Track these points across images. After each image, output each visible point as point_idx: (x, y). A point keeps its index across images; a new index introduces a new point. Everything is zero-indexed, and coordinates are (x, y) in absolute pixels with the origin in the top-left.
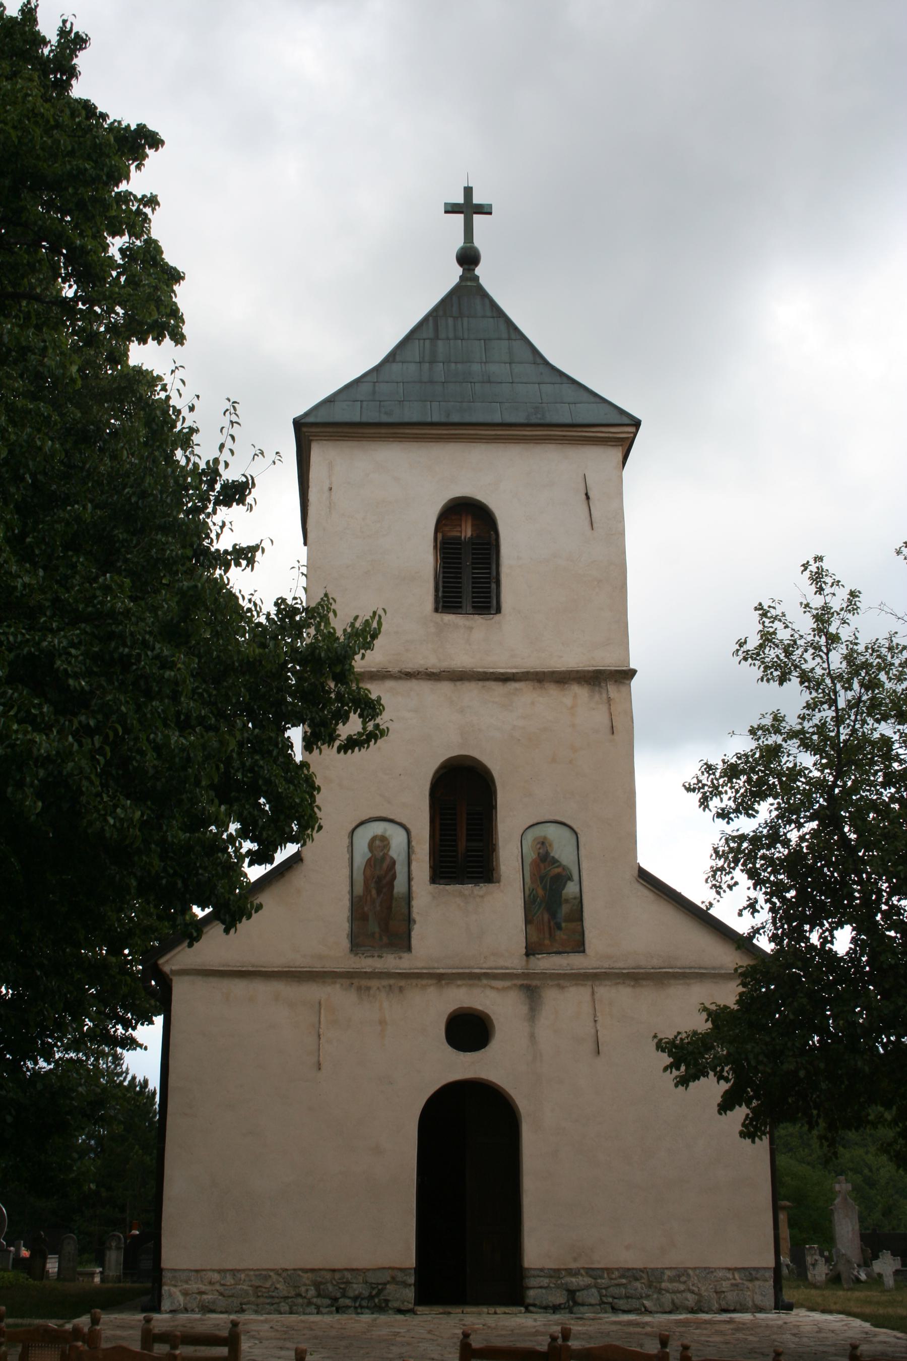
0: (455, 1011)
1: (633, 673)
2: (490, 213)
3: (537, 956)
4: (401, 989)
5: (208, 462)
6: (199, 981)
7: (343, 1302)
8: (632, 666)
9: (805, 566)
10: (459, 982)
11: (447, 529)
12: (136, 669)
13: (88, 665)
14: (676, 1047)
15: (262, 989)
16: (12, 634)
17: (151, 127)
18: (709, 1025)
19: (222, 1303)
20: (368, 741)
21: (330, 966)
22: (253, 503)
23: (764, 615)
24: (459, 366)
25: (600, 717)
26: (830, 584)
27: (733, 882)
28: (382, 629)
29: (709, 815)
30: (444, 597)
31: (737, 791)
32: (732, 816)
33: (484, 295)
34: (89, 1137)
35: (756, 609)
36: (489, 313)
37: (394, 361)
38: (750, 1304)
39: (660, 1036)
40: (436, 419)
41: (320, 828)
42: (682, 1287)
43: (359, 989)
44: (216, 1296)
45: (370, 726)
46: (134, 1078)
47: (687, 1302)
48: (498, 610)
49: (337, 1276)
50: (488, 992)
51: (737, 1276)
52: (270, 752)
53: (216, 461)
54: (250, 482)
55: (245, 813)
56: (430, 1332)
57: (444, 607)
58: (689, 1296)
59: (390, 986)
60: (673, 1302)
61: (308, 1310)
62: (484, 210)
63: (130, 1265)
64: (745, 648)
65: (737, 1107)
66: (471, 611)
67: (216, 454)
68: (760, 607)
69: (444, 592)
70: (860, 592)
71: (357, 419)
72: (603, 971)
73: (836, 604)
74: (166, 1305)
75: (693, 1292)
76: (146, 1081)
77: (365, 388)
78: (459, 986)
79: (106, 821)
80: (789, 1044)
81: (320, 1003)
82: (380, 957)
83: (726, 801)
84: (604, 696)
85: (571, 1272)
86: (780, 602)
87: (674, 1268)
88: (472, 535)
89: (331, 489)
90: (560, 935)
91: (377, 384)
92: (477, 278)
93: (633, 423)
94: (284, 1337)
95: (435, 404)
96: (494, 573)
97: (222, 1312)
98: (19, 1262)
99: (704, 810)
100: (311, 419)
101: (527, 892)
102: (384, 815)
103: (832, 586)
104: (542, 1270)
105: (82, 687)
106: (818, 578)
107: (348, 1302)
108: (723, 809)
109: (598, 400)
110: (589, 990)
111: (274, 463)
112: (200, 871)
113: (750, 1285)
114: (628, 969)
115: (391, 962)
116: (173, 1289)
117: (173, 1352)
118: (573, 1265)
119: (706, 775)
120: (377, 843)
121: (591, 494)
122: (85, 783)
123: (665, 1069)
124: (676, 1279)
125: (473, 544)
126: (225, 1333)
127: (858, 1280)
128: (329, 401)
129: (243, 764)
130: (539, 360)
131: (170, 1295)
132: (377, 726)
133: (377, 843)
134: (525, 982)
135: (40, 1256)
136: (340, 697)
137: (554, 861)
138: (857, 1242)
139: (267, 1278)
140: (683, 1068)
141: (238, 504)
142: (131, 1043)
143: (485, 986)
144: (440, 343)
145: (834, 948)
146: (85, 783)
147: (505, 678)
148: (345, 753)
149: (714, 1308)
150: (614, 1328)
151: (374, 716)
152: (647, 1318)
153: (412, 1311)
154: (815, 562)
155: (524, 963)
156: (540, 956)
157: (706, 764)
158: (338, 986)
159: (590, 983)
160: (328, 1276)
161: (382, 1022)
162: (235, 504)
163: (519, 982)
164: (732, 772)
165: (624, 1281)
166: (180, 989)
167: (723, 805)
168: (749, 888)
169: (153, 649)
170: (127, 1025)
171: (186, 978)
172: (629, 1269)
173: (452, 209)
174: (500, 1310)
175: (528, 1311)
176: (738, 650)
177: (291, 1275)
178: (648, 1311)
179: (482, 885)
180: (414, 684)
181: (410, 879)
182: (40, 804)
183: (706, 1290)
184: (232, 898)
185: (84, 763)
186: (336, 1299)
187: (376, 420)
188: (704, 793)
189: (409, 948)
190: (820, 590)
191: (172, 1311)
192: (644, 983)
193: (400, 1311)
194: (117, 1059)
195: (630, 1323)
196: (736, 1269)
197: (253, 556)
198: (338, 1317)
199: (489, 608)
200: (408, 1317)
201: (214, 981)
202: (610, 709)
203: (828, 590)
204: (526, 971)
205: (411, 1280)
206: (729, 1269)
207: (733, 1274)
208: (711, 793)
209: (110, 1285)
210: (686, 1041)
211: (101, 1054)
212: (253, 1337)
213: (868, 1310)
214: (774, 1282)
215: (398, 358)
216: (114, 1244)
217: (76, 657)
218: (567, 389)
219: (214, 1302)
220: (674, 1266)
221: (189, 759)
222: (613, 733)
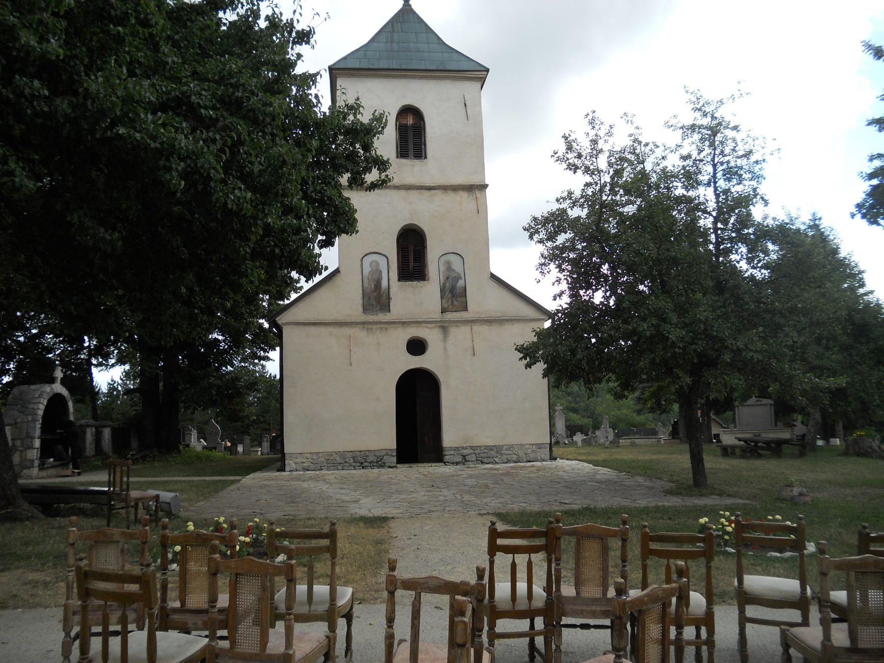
1: (487, 185)
5: (287, 20)
6: (295, 327)
7: (365, 464)
10: (412, 325)
11: (401, 120)
12: (246, 106)
13: (214, 103)
14: (525, 349)
15: (323, 330)
16: (165, 86)
19: (312, 467)
20: (382, 184)
21: (353, 319)
22: (314, 44)
24: (404, 44)
25: (472, 206)
33: (414, 13)
34: (254, 398)
36: (416, 21)
37: (374, 42)
38: (539, 458)
40: (395, 67)
41: (358, 231)
43: (367, 329)
44: (309, 464)
46: (271, 374)
48: (426, 158)
49: (362, 453)
50: (425, 329)
52: (330, 183)
53: (292, 19)
54: (312, 30)
55: (318, 215)
56: (405, 477)
58: (514, 456)
59: (381, 328)
60: (507, 459)
61: (350, 468)
63: (272, 447)
64: (557, 155)
66: (413, 157)
67: (291, 16)
71: (358, 66)
73: (601, 133)
74: (287, 468)
75: (515, 454)
77: (361, 53)
78: (412, 327)
79: (228, 197)
80: (579, 346)
81: (350, 336)
82: (377, 315)
84: (474, 196)
85: (463, 448)
92: (410, 6)
94: (341, 482)
96: (423, 141)
97: (312, 471)
98: (226, 448)
100: (336, 67)
102: (376, 251)
104: (451, 448)
105: (211, 115)
106: (592, 122)
107: (367, 464)
108: (541, 239)
112: (291, 243)
115: (382, 317)
116: (290, 462)
117: (289, 562)
118: (465, 446)
119: (533, 222)
120: (374, 264)
122: (212, 171)
125: (414, 127)
126: (326, 529)
127: (565, 444)
128: (345, 58)
129: (315, 189)
130: (441, 43)
131: (289, 464)
133: (374, 264)
135: (235, 445)
136: (366, 159)
137: (453, 270)
138: (564, 429)
139: (331, 455)
140: (528, 359)
141: (306, 44)
142: (267, 359)
143: (424, 327)
146: (212, 171)
147: (430, 188)
148: (370, 191)
150: (486, 471)
151: (385, 170)
152: (497, 466)
153: (395, 467)
155: (441, 316)
158: (358, 328)
159: (470, 324)
160: (359, 453)
161: (378, 344)
162: (304, 43)
165: (486, 451)
166: (286, 331)
167: (541, 237)
169: (257, 96)
170: (265, 351)
171: (289, 326)
172: (488, 446)
174: (433, 464)
175: (445, 465)
177: (342, 454)
178: (497, 463)
182: (183, 183)
183: (521, 453)
184: (310, 262)
185: (212, 159)
186: (362, 463)
189: (389, 311)
191: (290, 471)
192: (494, 323)
193: (390, 467)
194: (263, 367)
195: (491, 469)
196: (533, 444)
197: (316, 79)
198: (363, 470)
200: (394, 469)
201: (301, 327)
203: (597, 127)
205: (395, 454)
209: (264, 456)
211: (255, 365)
212: (328, 483)
213: (584, 458)
215: (376, 40)
216: (265, 440)
217: (206, 97)
218: (455, 56)
219: (309, 466)
221: (284, 162)
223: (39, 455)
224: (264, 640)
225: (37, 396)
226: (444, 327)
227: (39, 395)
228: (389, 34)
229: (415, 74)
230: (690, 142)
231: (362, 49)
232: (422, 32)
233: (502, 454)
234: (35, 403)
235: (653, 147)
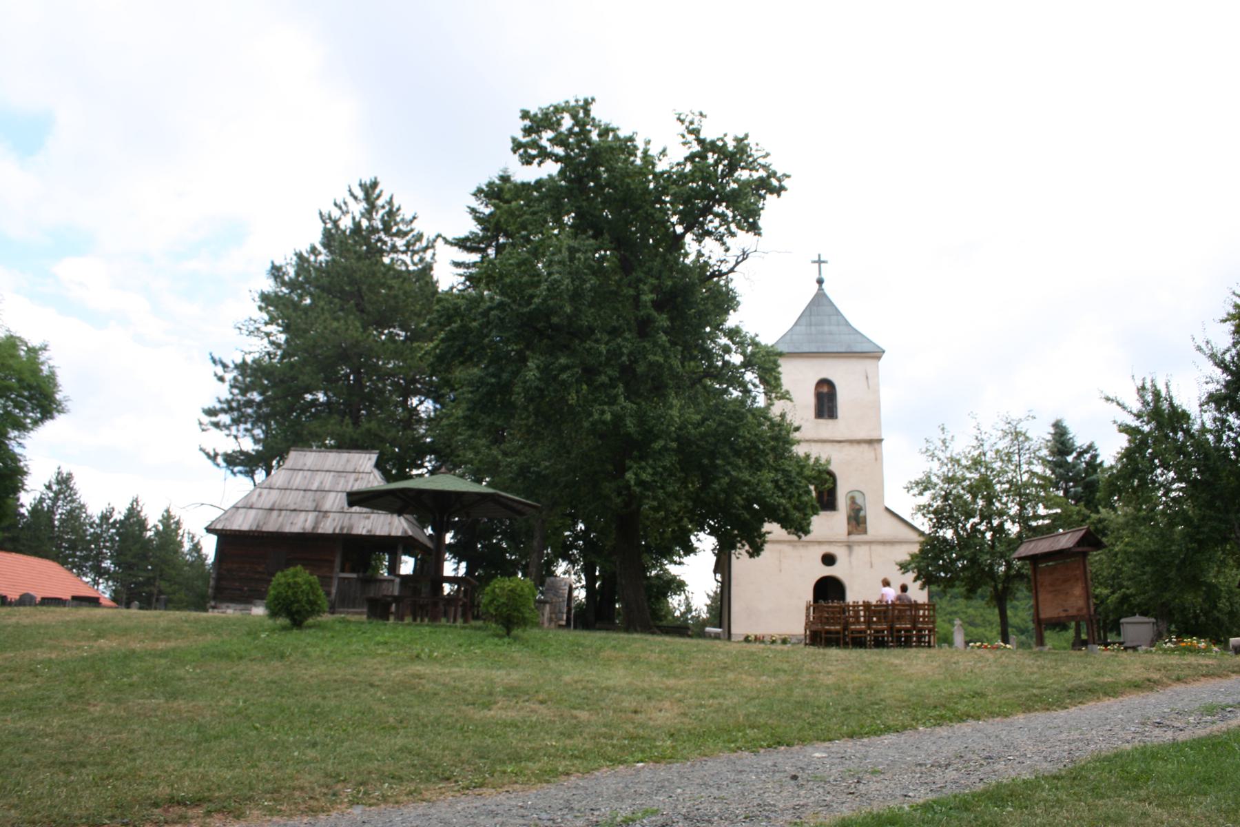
8: (883, 437)
48: (836, 418)
73: (949, 438)
76: (207, 556)
77: (788, 337)
90: (859, 529)
106: (943, 429)
161: (801, 557)
164: (917, 483)
173: (814, 262)
226: (849, 546)
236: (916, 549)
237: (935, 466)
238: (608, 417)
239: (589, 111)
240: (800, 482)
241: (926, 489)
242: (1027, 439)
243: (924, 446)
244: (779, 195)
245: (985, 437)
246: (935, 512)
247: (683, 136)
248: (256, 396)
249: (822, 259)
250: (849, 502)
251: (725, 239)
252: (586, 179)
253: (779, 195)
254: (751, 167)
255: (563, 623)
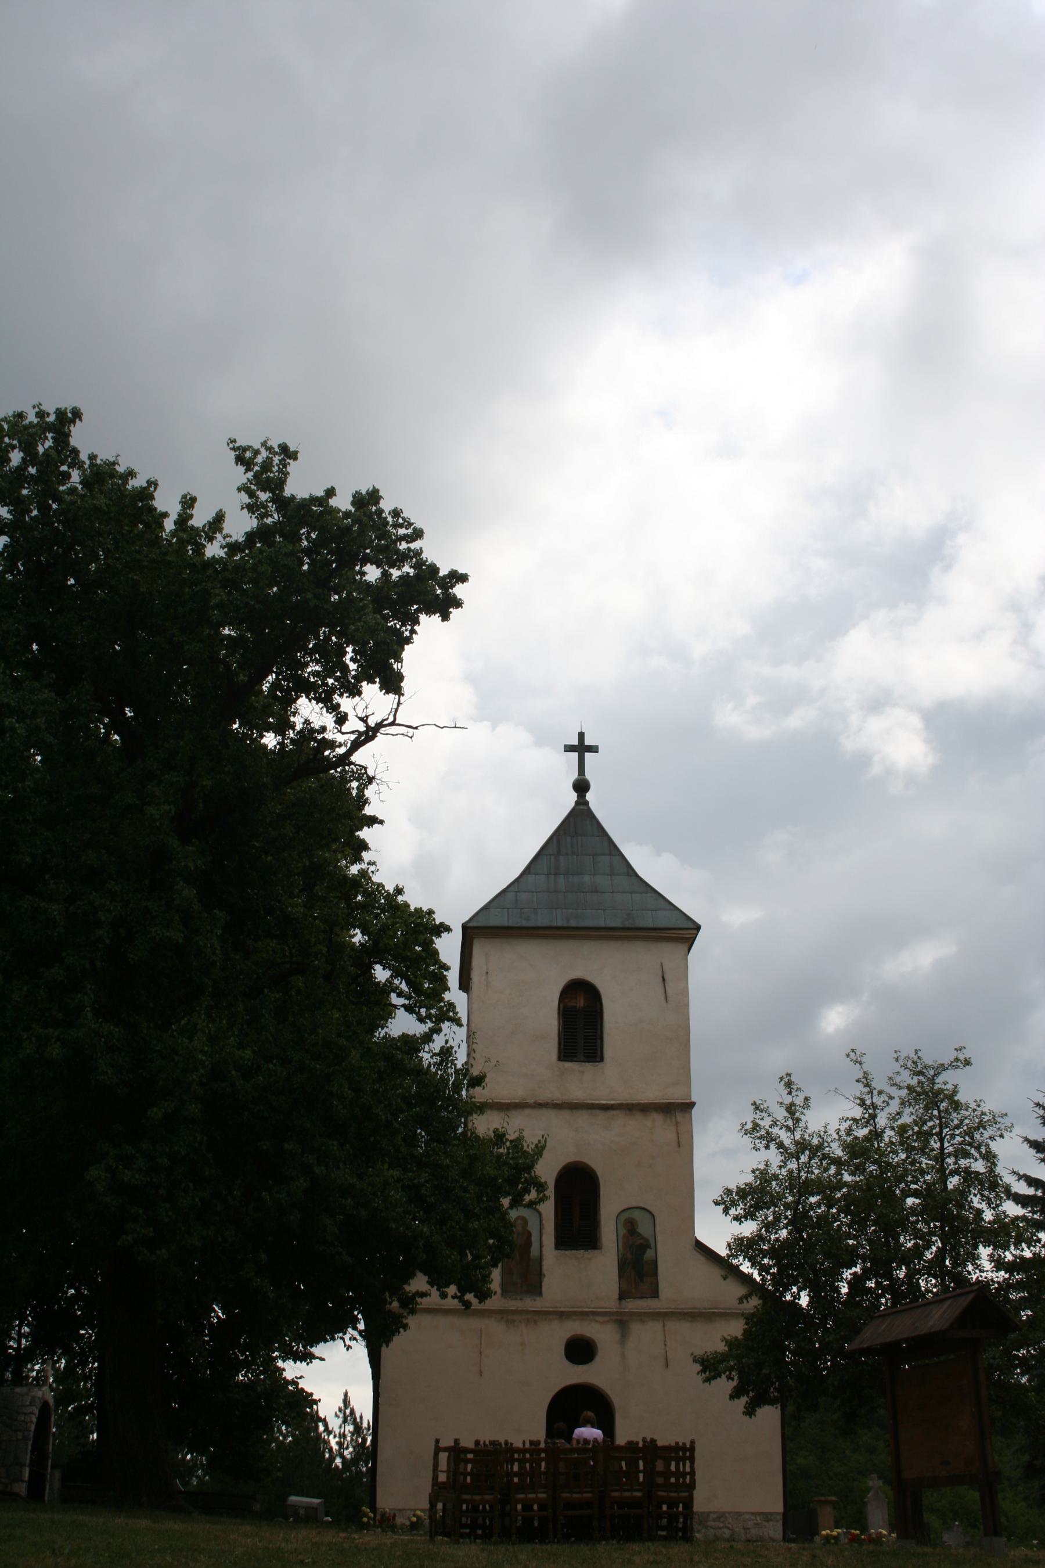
0: (572, 1336)
1: (693, 1104)
2: (597, 752)
3: (627, 1300)
4: (535, 1322)
8: (693, 1099)
9: (781, 1079)
10: (574, 1317)
17: (447, 923)
18: (726, 1349)
23: (757, 1108)
25: (670, 1135)
26: (795, 1089)
27: (739, 1263)
28: (547, 1145)
29: (729, 1218)
30: (564, 1049)
31: (746, 1205)
32: (742, 1219)
35: (752, 1104)
39: (695, 1354)
40: (560, 924)
42: (721, 1525)
45: (541, 1195)
47: (724, 1535)
48: (602, 1059)
51: (758, 1518)
57: (564, 1056)
62: (593, 749)
65: (742, 1397)
68: (754, 1104)
69: (564, 1045)
70: (810, 1098)
72: (670, 1310)
73: (799, 1101)
77: (510, 896)
81: (481, 1331)
82: (521, 1299)
83: (739, 1211)
86: (765, 1101)
87: (716, 1512)
88: (584, 1005)
89: (487, 973)
91: (518, 893)
92: (587, 803)
93: (695, 927)
95: (559, 911)
96: (599, 1053)
99: (726, 1216)
101: (620, 1256)
103: (796, 1091)
106: (789, 1085)
108: (737, 1216)
109: (672, 907)
110: (661, 1324)
111: (496, 1066)
113: (767, 1524)
114: (688, 1309)
115: (530, 1303)
121: (666, 977)
123: (698, 1373)
124: (718, 1519)
132: (544, 1195)
134: (619, 1318)
137: (639, 1235)
140: (707, 1373)
144: (562, 858)
145: (800, 1302)
149: (742, 1539)
151: (542, 1191)
154: (787, 1077)
156: (628, 1300)
157: (727, 1189)
163: (615, 1317)
167: (737, 1213)
168: (748, 1267)
173: (569, 748)
176: (741, 1129)
179: (589, 1251)
180: (545, 1112)
181: (541, 1246)
187: (519, 925)
188: (726, 1205)
189: (540, 1294)
190: (790, 1093)
199: (596, 1057)
202: (677, 1129)
203: (794, 1093)
204: (618, 1310)
206: (753, 1514)
207: (756, 1517)
208: (730, 1205)
210: (710, 1357)
214: (783, 1522)
220: (716, 1510)
222: (679, 1146)
223: (26, 1493)
224: (512, 1468)
225: (28, 1403)
226: (622, 1322)
227: (31, 1403)
228: (553, 857)
229: (591, 933)
230: (909, 1113)
231: (512, 888)
232: (604, 855)
233: (707, 1527)
234: (26, 1414)
235: (887, 1099)
236: (736, 1329)
237: (773, 1157)
238: (55, 1051)
239: (68, 435)
240: (466, 1190)
241: (757, 1207)
242: (957, 1106)
243: (749, 1117)
244: (445, 617)
245: (878, 1100)
246: (772, 1253)
247: (251, 494)
248: (100, 1020)
249: (575, 742)
250: (622, 1231)
251: (336, 698)
252: (351, 597)
253: (445, 617)
254: (388, 555)
255: (22, 1489)
